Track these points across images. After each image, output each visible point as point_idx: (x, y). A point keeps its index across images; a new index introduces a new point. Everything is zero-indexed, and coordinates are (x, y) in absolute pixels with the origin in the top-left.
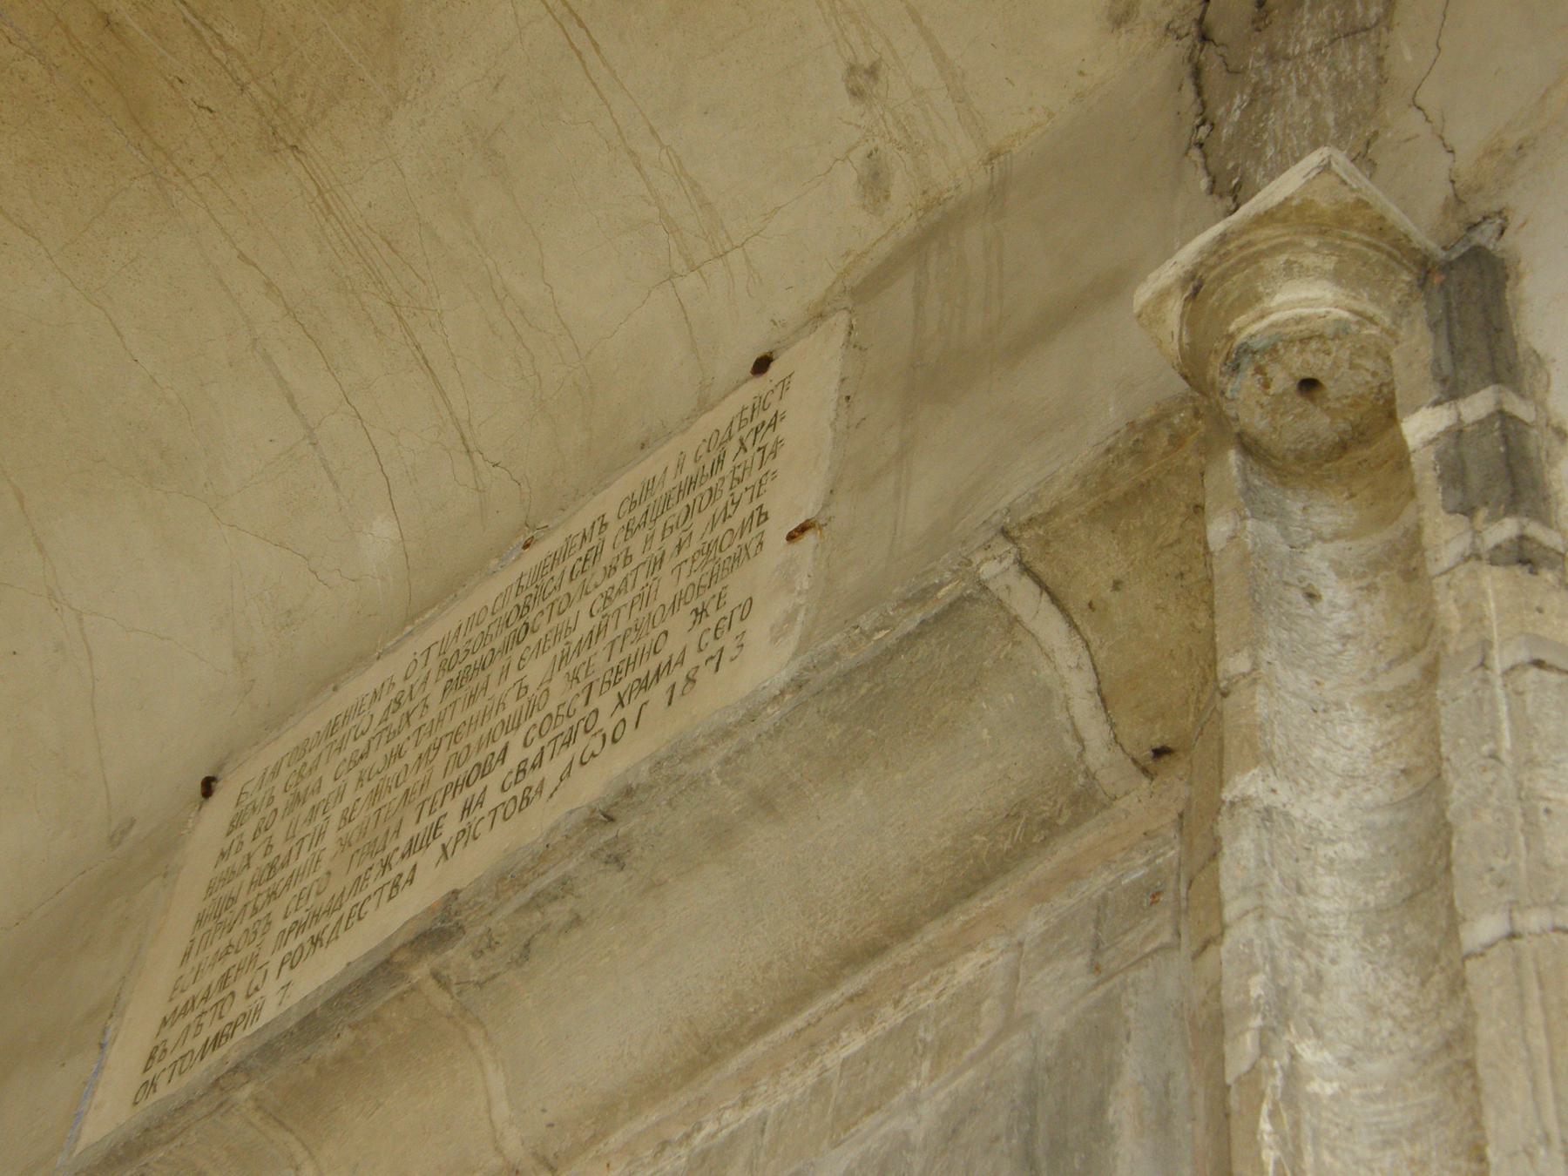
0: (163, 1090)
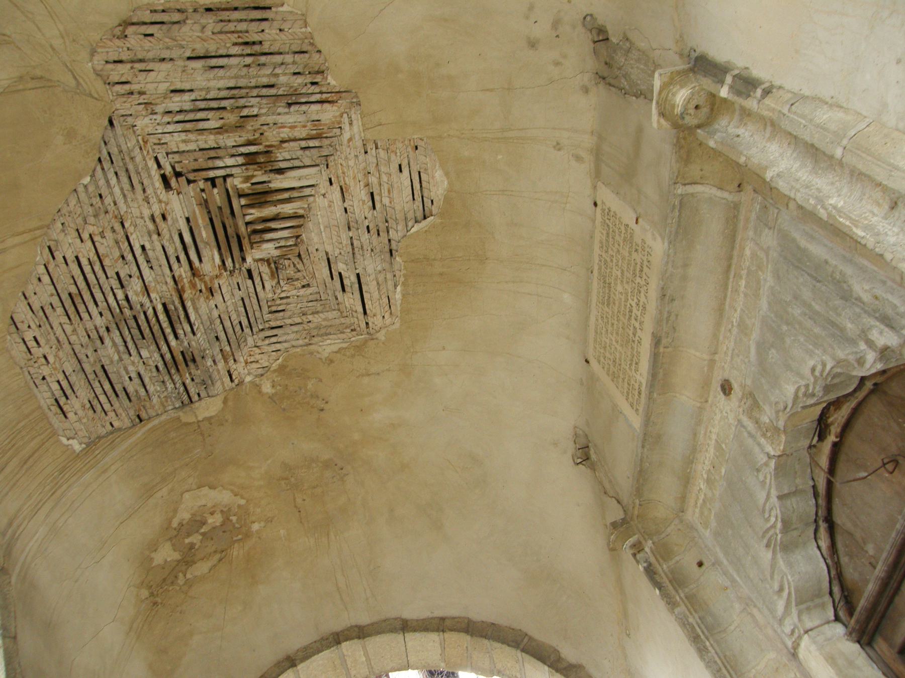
0: (641, 409)
